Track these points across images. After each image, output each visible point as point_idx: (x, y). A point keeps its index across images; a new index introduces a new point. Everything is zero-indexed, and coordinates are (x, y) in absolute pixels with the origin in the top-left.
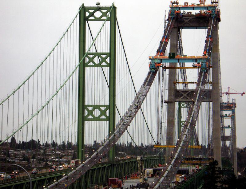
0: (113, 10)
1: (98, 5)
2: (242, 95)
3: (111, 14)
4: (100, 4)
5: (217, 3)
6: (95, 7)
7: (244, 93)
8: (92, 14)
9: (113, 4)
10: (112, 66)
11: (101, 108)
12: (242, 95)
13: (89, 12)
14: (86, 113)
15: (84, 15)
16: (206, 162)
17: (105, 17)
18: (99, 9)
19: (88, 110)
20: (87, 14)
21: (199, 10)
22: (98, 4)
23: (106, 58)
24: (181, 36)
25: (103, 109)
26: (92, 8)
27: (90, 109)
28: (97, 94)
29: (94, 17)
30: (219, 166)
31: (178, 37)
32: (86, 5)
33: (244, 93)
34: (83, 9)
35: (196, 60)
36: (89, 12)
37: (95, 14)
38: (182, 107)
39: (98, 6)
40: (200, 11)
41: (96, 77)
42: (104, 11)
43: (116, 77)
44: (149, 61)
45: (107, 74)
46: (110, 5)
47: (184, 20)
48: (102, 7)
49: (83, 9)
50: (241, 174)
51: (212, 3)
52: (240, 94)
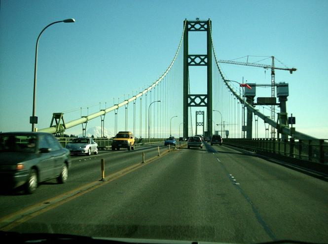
0: (208, 23)
2: (291, 73)
3: (207, 26)
7: (295, 70)
8: (193, 26)
11: (194, 104)
12: (291, 73)
13: (191, 25)
14: (206, 101)
15: (189, 27)
18: (198, 22)
19: (191, 98)
21: (213, 146)
23: (205, 98)
24: (208, 241)
25: (203, 97)
27: (203, 104)
28: (198, 74)
29: (195, 28)
31: (187, 33)
32: (188, 20)
33: (295, 70)
35: (274, 82)
36: (191, 25)
37: (200, 26)
38: (189, 30)
40: (212, 145)
41: (198, 86)
46: (206, 19)
49: (187, 23)
50: (291, 137)
52: (288, 70)
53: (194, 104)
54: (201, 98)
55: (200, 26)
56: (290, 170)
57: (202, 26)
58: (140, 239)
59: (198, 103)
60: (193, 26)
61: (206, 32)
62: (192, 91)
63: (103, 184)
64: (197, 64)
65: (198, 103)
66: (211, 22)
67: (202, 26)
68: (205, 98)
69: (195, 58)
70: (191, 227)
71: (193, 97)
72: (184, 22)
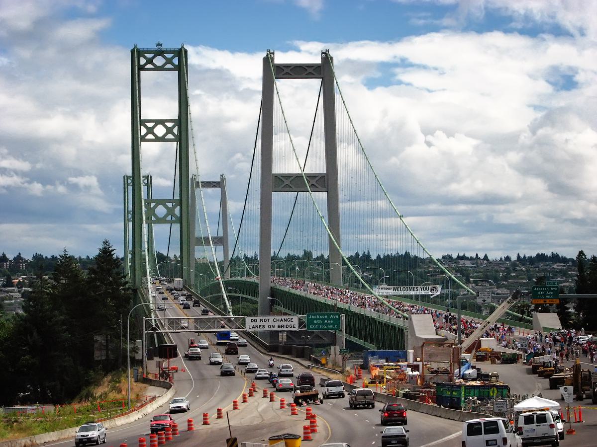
0: (181, 54)
1: (159, 47)
3: (178, 61)
4: (161, 45)
5: (124, 177)
6: (154, 50)
8: (150, 61)
11: (154, 138)
13: (145, 58)
16: (389, 237)
17: (150, 65)
18: (160, 53)
22: (160, 45)
25: (170, 125)
26: (149, 51)
30: (565, 437)
32: (141, 46)
37: (164, 61)
38: (142, 68)
39: (159, 48)
42: (169, 56)
43: (260, 176)
44: (300, 253)
45: (236, 233)
47: (492, 389)
48: (165, 49)
51: (148, 177)
53: (154, 138)
54: (165, 127)
55: (164, 61)
56: (136, 262)
57: (169, 61)
58: (131, 246)
60: (150, 61)
61: (177, 72)
63: (473, 318)
64: (162, 122)
65: (160, 127)
67: (169, 61)
68: (173, 127)
69: (165, 64)
70: (385, 324)
72: (132, 52)
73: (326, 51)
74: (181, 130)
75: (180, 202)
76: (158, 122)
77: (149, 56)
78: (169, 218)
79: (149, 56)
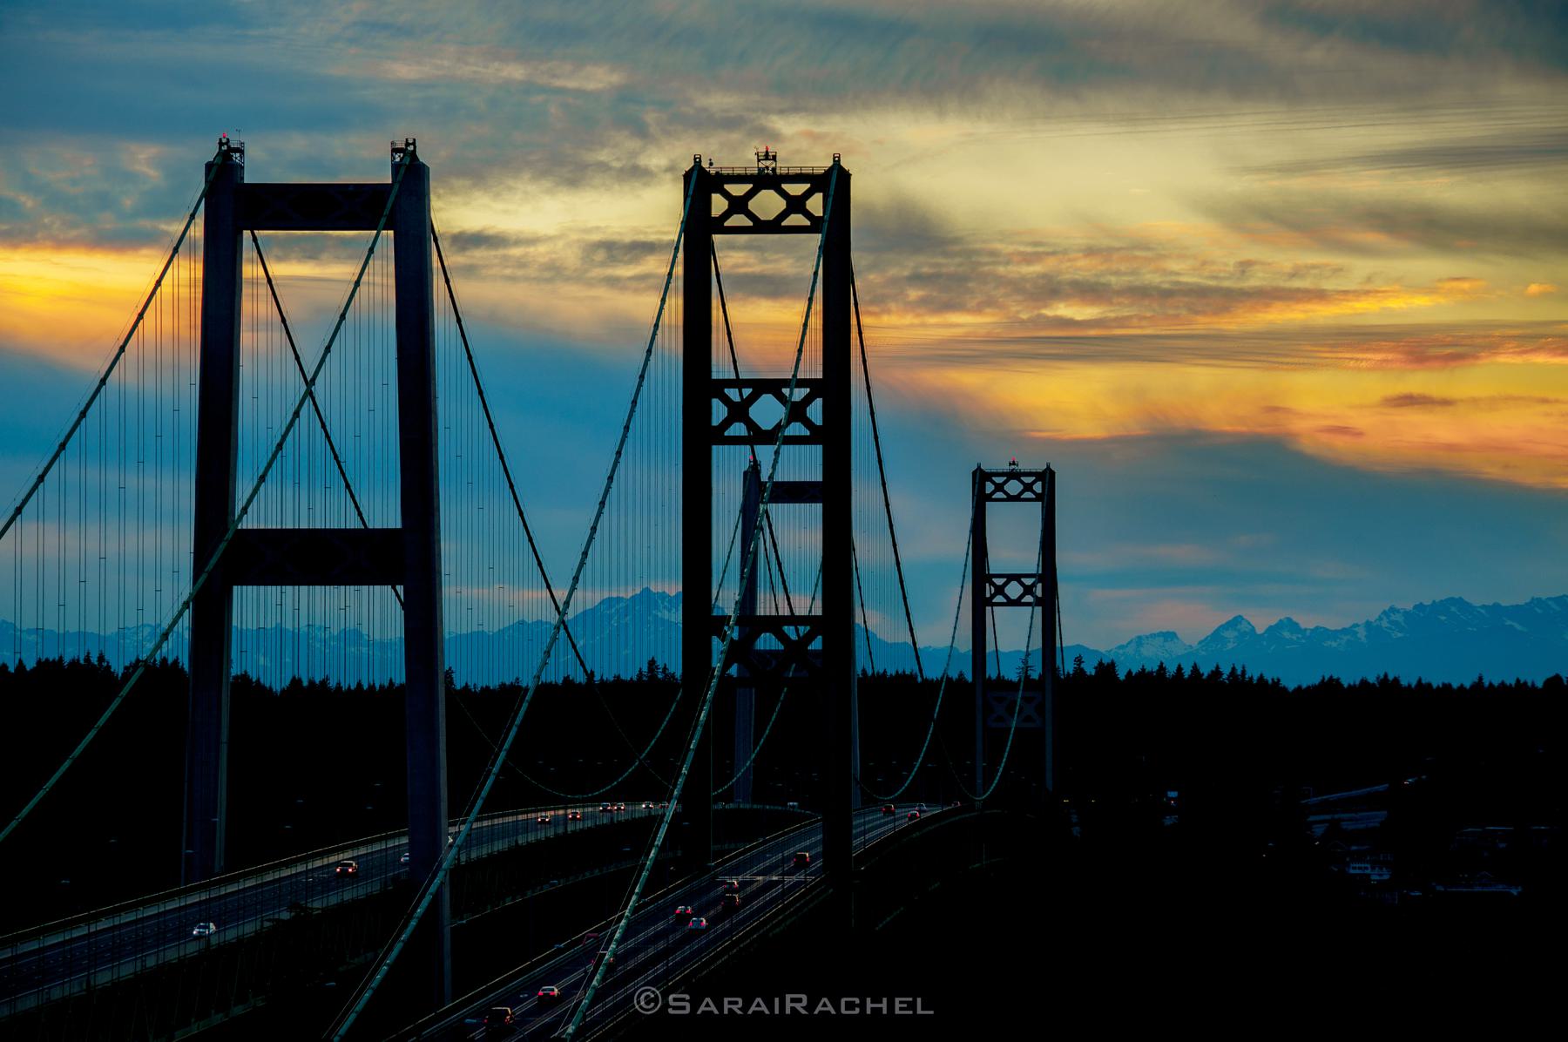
1: (768, 163)
4: (774, 158)
8: (739, 205)
9: (837, 162)
10: (1048, 605)
13: (726, 195)
15: (709, 208)
18: (1013, 475)
20: (719, 204)
25: (1028, 582)
34: (981, 477)
36: (726, 195)
37: (752, 205)
38: (719, 226)
46: (1041, 467)
49: (981, 477)
57: (796, 205)
59: (767, 400)
60: (999, 487)
62: (999, 561)
66: (1052, 474)
71: (999, 582)
72: (974, 473)
73: (407, 144)
74: (1045, 589)
75: (1040, 578)
76: (1011, 578)
77: (738, 190)
78: (747, 392)
79: (738, 190)
